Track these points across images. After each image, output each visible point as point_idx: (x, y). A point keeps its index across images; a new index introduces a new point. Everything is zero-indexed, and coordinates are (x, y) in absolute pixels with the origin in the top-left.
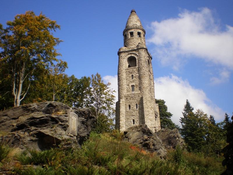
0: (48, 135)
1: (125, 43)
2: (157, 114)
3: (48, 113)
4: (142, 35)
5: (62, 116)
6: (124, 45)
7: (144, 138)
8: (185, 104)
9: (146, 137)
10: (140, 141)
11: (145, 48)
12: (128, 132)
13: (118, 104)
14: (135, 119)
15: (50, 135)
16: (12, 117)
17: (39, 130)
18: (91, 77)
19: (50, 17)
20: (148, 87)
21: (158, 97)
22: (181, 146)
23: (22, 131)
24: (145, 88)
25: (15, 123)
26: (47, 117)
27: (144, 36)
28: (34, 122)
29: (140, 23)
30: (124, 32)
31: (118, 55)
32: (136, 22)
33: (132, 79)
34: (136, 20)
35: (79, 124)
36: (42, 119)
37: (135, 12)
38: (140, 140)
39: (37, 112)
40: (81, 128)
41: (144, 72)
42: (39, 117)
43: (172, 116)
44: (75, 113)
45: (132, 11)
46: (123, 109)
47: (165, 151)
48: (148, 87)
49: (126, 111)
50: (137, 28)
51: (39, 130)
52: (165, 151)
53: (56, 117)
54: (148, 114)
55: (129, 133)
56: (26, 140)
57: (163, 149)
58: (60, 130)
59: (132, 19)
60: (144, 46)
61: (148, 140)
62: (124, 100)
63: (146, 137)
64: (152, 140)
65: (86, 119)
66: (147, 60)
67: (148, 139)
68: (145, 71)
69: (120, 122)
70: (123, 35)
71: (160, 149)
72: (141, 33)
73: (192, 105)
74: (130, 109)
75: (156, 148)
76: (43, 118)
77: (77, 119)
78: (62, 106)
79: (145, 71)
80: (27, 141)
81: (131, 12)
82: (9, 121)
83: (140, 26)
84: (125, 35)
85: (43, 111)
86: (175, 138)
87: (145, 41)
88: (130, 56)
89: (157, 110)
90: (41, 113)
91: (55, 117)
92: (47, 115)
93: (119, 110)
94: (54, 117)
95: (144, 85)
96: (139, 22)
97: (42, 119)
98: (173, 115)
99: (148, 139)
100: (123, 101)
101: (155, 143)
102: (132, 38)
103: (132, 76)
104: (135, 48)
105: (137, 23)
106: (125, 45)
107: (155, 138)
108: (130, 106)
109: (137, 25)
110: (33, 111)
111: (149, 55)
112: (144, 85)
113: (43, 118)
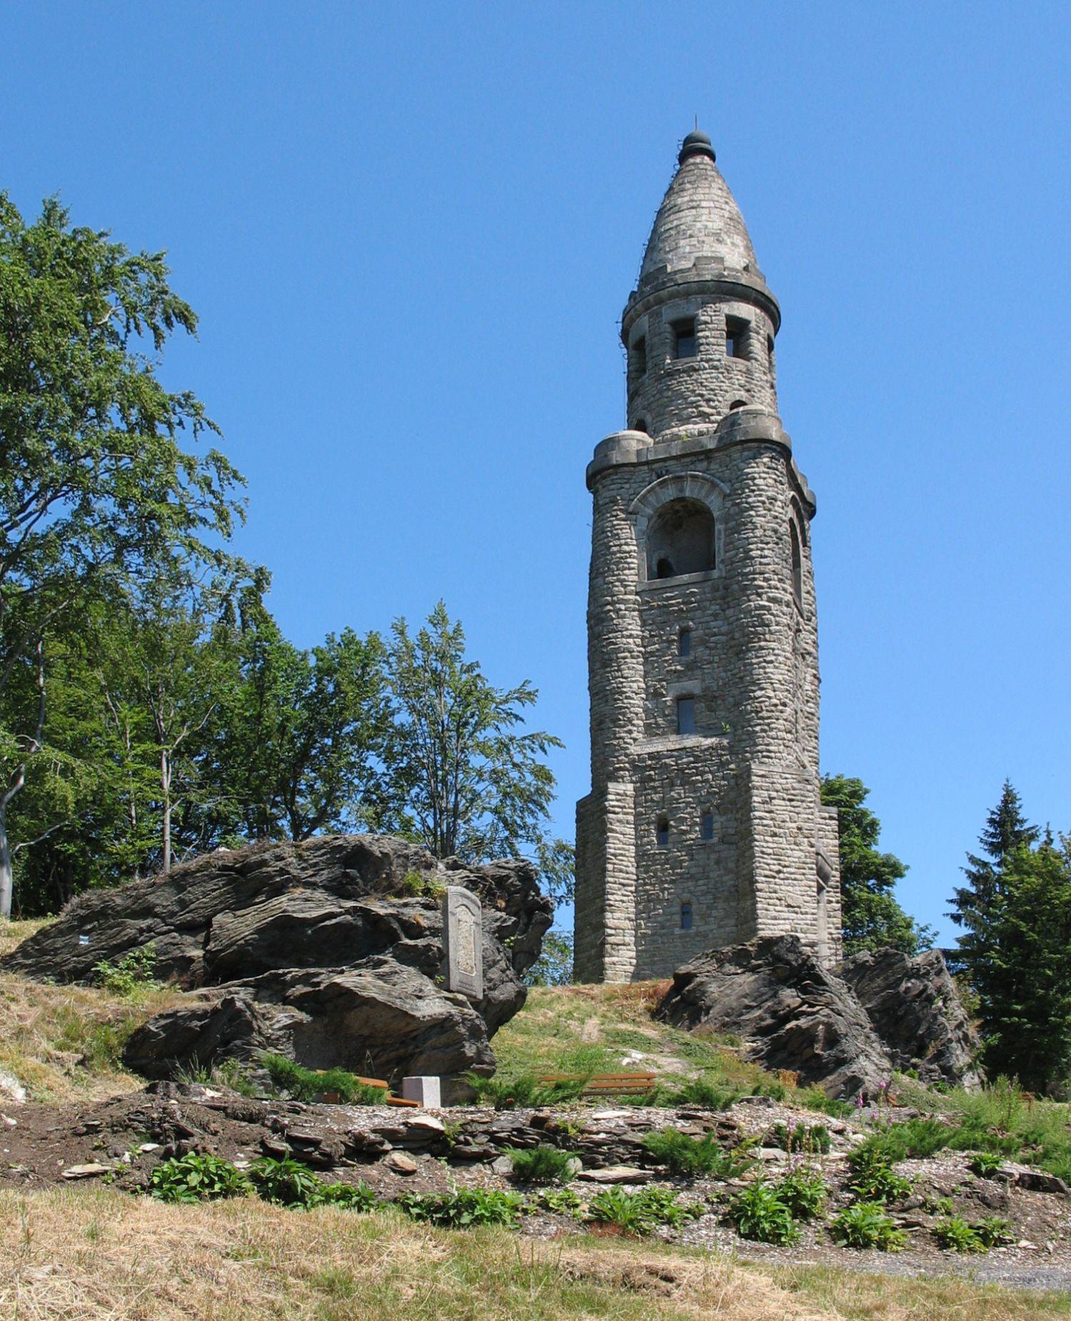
0: (371, 1002)
1: (638, 400)
2: (827, 868)
3: (348, 897)
4: (757, 345)
5: (413, 906)
6: (630, 412)
7: (780, 1003)
8: (995, 801)
9: (790, 997)
10: (761, 1019)
11: (775, 436)
12: (695, 976)
13: (591, 815)
14: (694, 900)
15: (380, 998)
16: (176, 920)
17: (327, 977)
18: (389, 640)
19: (115, 218)
20: (784, 705)
21: (837, 766)
22: (954, 1045)
23: (245, 985)
24: (764, 714)
25: (196, 945)
26: (347, 912)
27: (771, 347)
28: (288, 940)
29: (748, 248)
30: (632, 320)
31: (589, 487)
32: (720, 241)
33: (683, 651)
34: (717, 224)
35: (487, 942)
36: (328, 923)
37: (713, 157)
38: (758, 1013)
39: (298, 892)
40: (495, 963)
41: (763, 607)
42: (314, 914)
43: (901, 876)
44: (466, 887)
45: (688, 140)
46: (622, 841)
47: (883, 1070)
48: (784, 705)
49: (641, 856)
50: (729, 290)
51: (327, 977)
52: (883, 1070)
53: (390, 911)
54: (776, 868)
55: (702, 983)
56: (276, 1026)
57: (875, 1058)
58: (411, 978)
59: (687, 216)
60: (767, 429)
61: (803, 1013)
62: (630, 787)
63: (789, 1001)
64: (828, 1016)
65: (514, 919)
66: (785, 528)
67: (804, 1008)
68: (771, 600)
69: (608, 915)
70: (625, 335)
71: (862, 1058)
72: (753, 325)
73: (1031, 814)
74: (663, 840)
75: (843, 1051)
76: (334, 921)
77: (480, 921)
78: (406, 857)
79: (771, 600)
80: (280, 1029)
81: (683, 158)
82: (166, 939)
83: (746, 269)
84: (631, 341)
85: (324, 887)
86: (930, 1000)
87: (772, 387)
88: (670, 493)
89: (829, 844)
90: (319, 894)
91: (387, 915)
92: (349, 904)
93: (602, 843)
94: (382, 912)
95: (759, 693)
96: (738, 240)
97: (328, 923)
98: (907, 867)
99: (804, 1008)
100: (621, 790)
101: (841, 1027)
102: (683, 363)
103: (684, 632)
104: (704, 439)
105: (722, 250)
106: (641, 414)
107: (840, 1006)
108: (663, 827)
109: (721, 260)
110: (278, 890)
111: (797, 487)
112: (759, 693)
113: (334, 921)
